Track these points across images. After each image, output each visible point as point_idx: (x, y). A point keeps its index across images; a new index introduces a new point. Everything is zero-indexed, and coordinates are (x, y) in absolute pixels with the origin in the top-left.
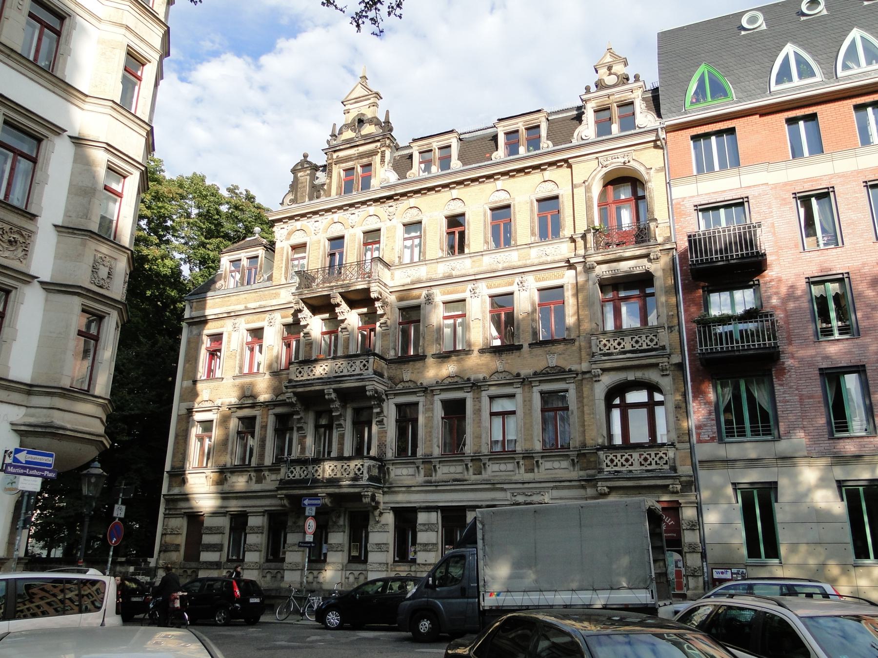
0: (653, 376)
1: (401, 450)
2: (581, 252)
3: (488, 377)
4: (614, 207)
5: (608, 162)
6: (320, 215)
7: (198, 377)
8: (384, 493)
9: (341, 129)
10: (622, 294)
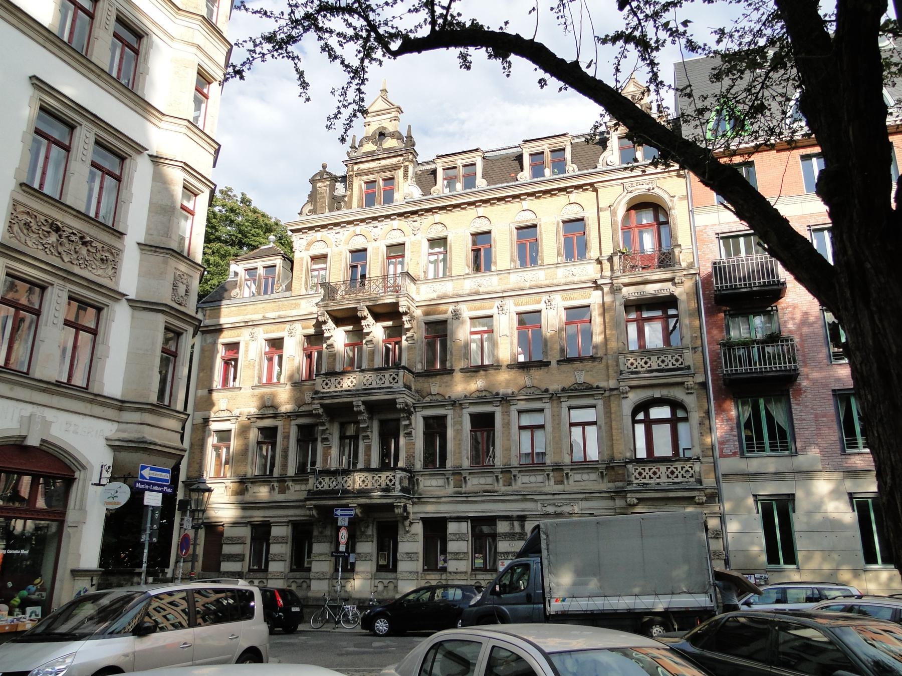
0: (678, 394)
1: (429, 460)
2: (607, 273)
3: (517, 392)
4: (637, 230)
5: (633, 188)
6: (342, 227)
7: (214, 387)
8: (414, 504)
10: (645, 315)
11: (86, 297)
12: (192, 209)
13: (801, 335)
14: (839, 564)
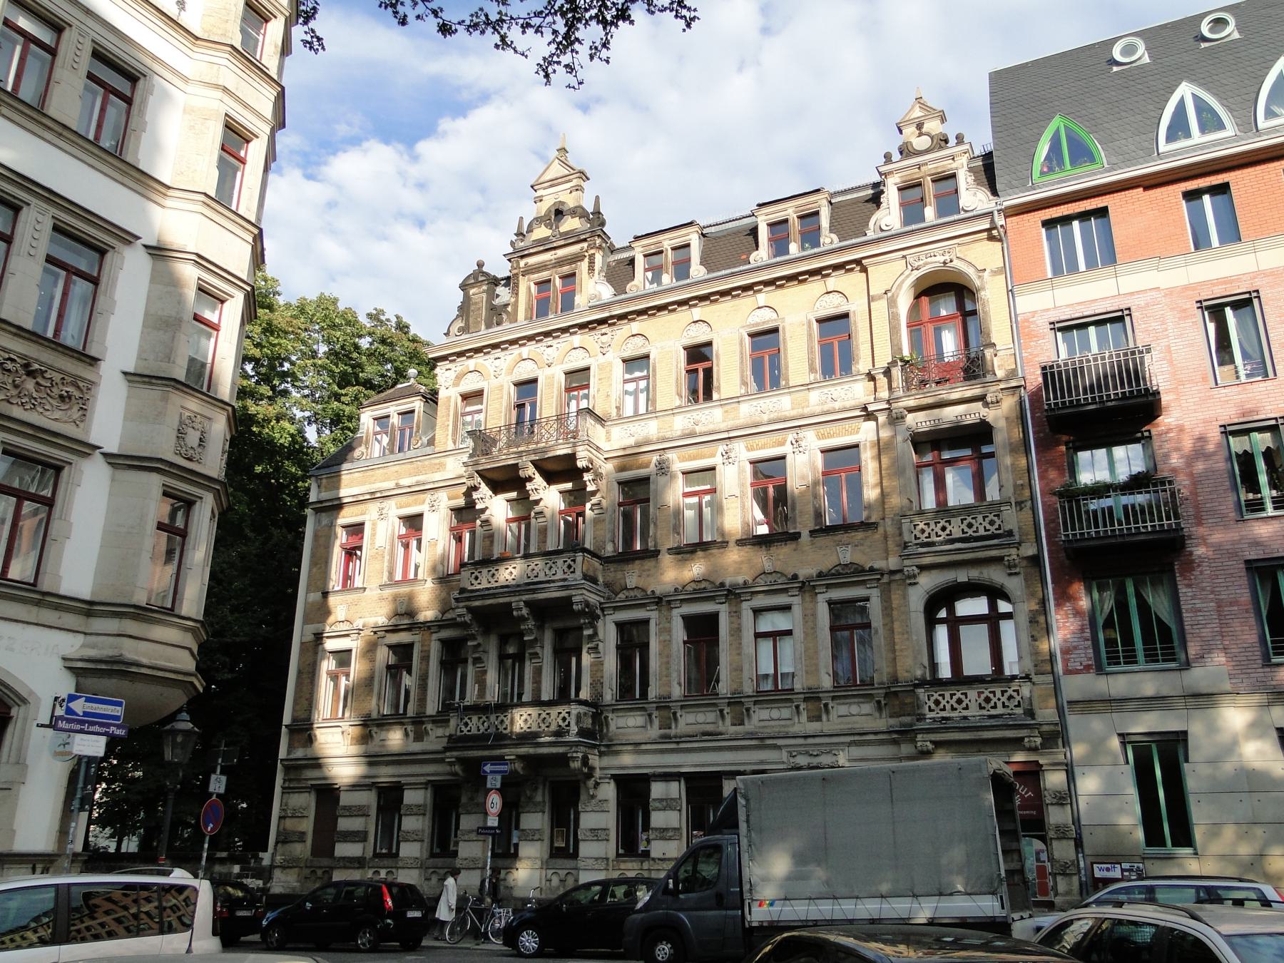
0: (995, 575)
1: (625, 690)
2: (884, 394)
3: (751, 581)
4: (931, 327)
5: (921, 262)
6: (503, 350)
8: (601, 754)
9: (530, 225)
10: (946, 455)
11: (17, 447)
12: (216, 322)
13: (1191, 475)
14: (1267, 844)
